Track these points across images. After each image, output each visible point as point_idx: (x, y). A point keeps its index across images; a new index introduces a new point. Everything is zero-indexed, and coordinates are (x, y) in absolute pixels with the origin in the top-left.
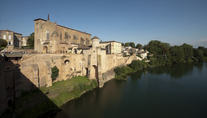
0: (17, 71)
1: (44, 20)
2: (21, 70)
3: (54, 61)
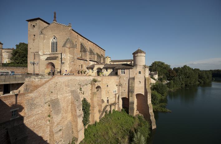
0: (16, 124)
1: (45, 22)
2: (25, 118)
3: (83, 89)
